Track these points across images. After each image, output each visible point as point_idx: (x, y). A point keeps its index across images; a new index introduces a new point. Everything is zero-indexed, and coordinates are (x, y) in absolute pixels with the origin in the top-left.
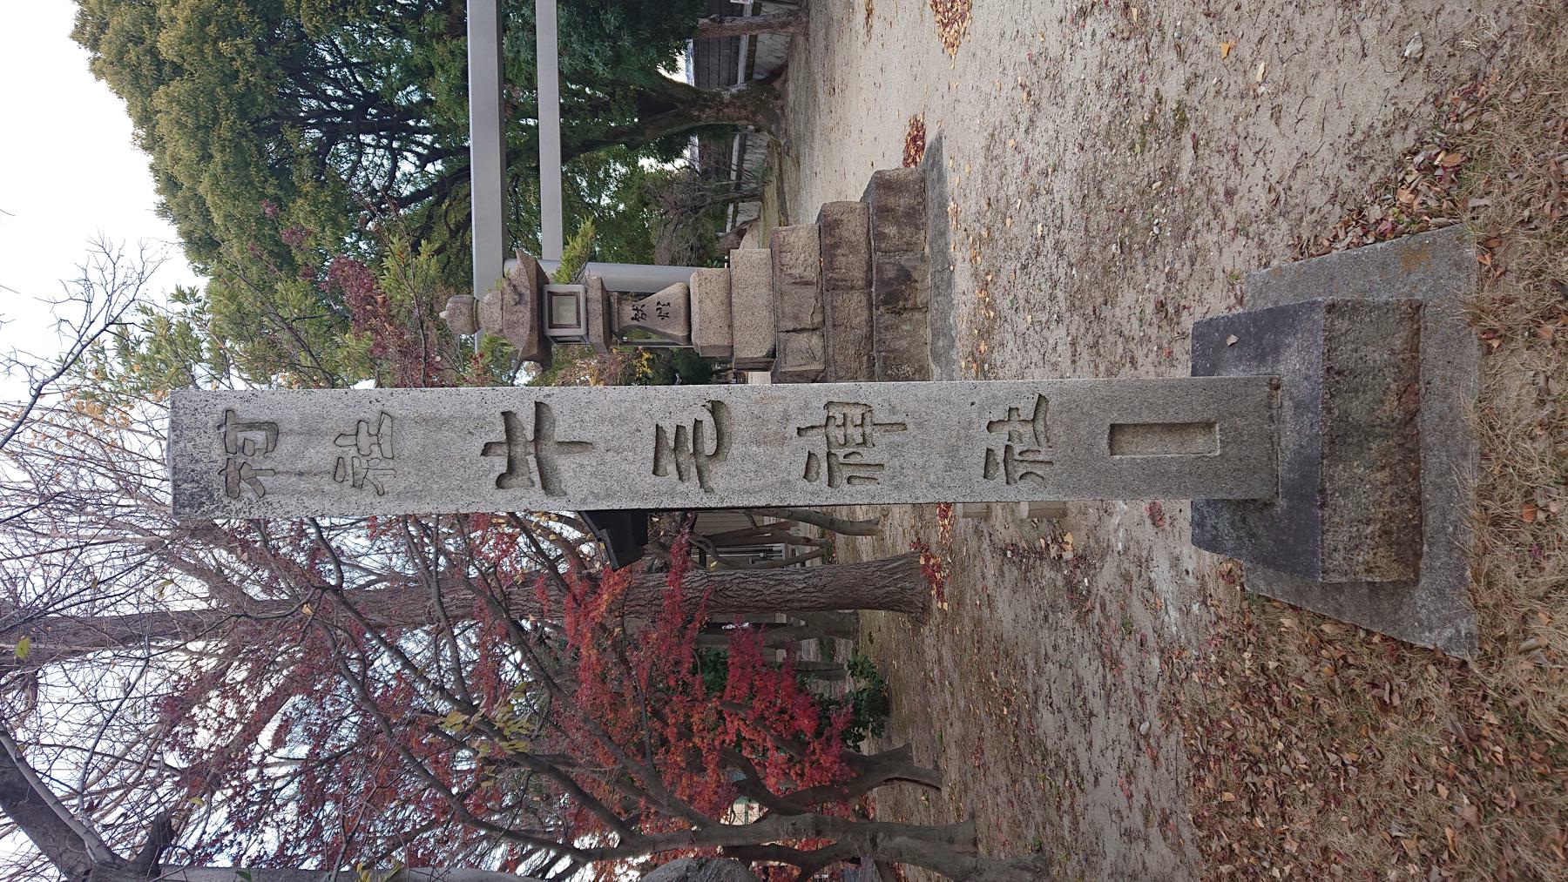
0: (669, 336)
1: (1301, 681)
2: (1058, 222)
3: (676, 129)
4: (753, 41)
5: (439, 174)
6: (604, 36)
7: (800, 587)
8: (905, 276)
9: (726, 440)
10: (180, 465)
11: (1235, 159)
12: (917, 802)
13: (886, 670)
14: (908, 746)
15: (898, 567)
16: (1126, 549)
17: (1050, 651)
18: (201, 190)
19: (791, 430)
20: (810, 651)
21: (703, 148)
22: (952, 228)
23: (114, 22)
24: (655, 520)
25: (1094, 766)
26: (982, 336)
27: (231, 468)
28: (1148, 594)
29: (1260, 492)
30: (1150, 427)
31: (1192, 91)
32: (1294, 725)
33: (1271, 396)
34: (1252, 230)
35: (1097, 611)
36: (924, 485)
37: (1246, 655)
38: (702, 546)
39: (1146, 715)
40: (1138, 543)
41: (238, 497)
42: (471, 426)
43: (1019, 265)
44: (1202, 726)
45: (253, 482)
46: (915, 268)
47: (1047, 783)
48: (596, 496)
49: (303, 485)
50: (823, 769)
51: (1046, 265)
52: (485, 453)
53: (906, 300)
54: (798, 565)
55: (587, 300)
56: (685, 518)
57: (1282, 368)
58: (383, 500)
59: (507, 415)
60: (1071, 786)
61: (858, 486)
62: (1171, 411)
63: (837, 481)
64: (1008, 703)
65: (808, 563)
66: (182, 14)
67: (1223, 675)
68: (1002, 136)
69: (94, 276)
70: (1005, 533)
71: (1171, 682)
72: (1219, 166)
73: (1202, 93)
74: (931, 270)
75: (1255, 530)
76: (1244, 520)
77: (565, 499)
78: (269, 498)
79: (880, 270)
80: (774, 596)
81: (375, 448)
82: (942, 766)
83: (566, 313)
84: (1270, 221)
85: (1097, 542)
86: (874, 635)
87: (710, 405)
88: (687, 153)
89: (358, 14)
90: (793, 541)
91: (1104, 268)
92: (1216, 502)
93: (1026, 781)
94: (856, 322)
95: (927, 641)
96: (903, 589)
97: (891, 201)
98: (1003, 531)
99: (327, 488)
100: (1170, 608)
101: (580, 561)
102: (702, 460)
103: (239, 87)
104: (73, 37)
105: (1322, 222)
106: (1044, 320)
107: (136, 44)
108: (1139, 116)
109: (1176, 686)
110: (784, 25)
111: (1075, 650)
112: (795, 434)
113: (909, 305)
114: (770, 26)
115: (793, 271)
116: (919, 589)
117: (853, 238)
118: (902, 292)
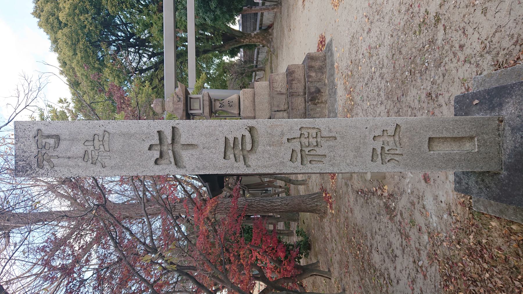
0: (231, 113)
1: (499, 249)
2: (381, 66)
3: (236, 46)
4: (262, 15)
5: (156, 62)
6: (210, 10)
7: (279, 204)
8: (318, 91)
9: (256, 144)
10: (18, 154)
11: (464, 32)
12: (322, 282)
13: (310, 234)
14: (318, 262)
15: (315, 197)
16: (412, 192)
17: (377, 230)
18: (73, 65)
19: (285, 139)
20: (281, 226)
21: (245, 52)
22: (336, 73)
23: (45, 9)
24: (227, 179)
25: (397, 277)
26: (348, 112)
27: (40, 155)
28: (423, 210)
29: (494, 167)
30: (446, 138)
31: (442, 7)
32: (496, 267)
33: (499, 125)
34: (472, 61)
35: (399, 216)
36: (344, 164)
37: (471, 237)
38: (244, 188)
39: (421, 258)
40: (418, 190)
41: (42, 168)
42: (144, 137)
43: (364, 84)
44: (448, 264)
45: (49, 161)
46: (322, 88)
47: (376, 281)
48: (199, 169)
49: (70, 163)
50: (288, 271)
51: (376, 83)
52: (150, 149)
53: (319, 99)
54: (277, 196)
55: (203, 100)
56: (238, 179)
57: (504, 113)
58: (104, 169)
59: (159, 132)
60: (386, 283)
61: (315, 165)
62: (456, 132)
63: (305, 162)
64: (359, 250)
65: (280, 195)
66: (67, 6)
67: (459, 244)
68: (357, 36)
69: (21, 89)
70: (358, 185)
71: (433, 246)
72: (456, 37)
73: (447, 8)
74: (328, 89)
75: (489, 185)
76: (483, 180)
77: (185, 170)
78: (56, 168)
79: (309, 89)
80: (270, 207)
81: (102, 147)
82: (332, 269)
83: (196, 105)
84: (482, 56)
85: (399, 189)
86: (305, 221)
87: (249, 129)
88: (239, 55)
89: (126, 7)
90: (276, 187)
91: (402, 81)
92: (467, 173)
93: (367, 279)
94: (300, 108)
95: (326, 224)
96: (317, 205)
97: (313, 64)
98: (357, 184)
99: (80, 164)
100: (433, 217)
101: (200, 195)
102: (245, 153)
103: (86, 31)
104: (33, 14)
105: (510, 54)
106: (375, 104)
107: (52, 16)
108: (418, 20)
109: (435, 248)
110: (273, 9)
111: (388, 231)
112: (286, 141)
113: (320, 101)
114: (268, 9)
115: (277, 89)
116: (323, 205)
117: (299, 77)
118: (317, 97)
